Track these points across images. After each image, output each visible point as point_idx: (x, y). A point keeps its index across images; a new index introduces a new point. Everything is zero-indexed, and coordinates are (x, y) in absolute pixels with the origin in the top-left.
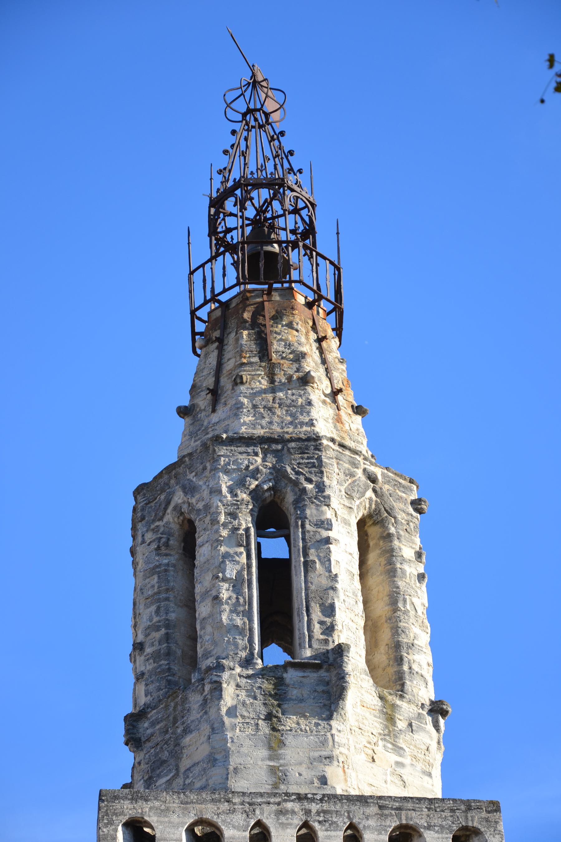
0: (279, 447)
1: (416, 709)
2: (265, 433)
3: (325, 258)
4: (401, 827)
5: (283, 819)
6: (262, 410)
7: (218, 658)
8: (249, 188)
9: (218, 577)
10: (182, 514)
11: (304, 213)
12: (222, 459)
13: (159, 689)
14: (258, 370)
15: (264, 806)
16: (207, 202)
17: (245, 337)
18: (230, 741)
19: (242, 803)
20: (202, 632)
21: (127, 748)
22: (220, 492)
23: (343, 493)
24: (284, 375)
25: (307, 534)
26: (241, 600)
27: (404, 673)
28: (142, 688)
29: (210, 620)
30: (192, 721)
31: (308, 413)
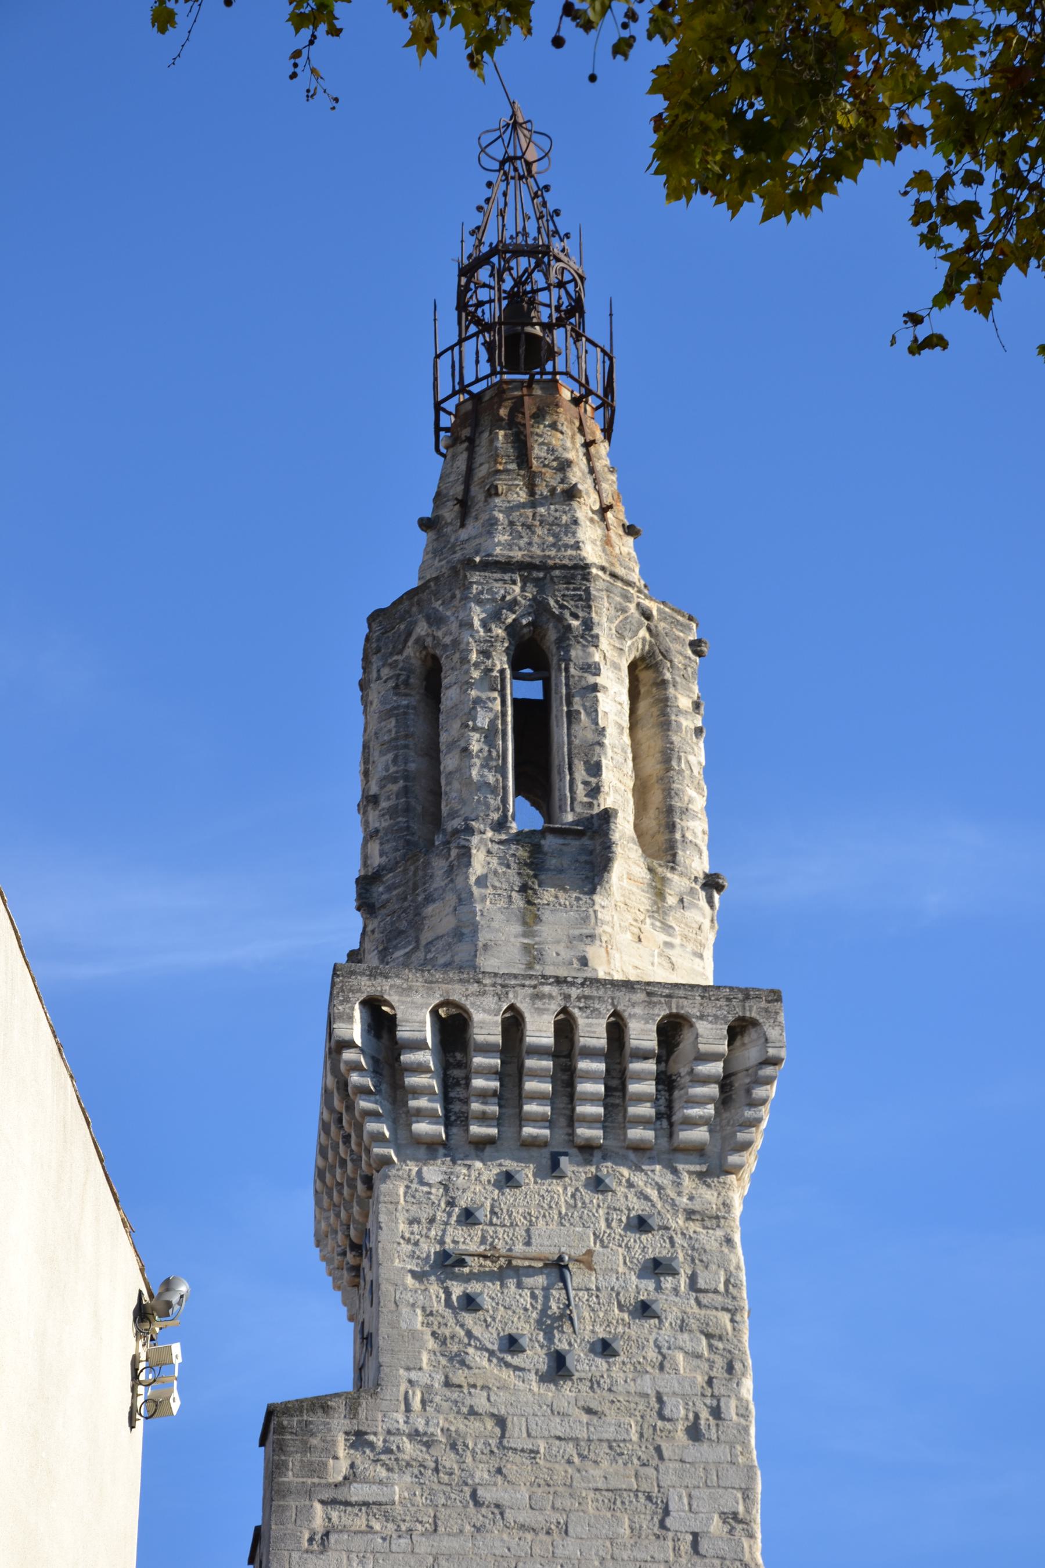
0: (541, 575)
1: (688, 882)
2: (523, 556)
3: (596, 345)
4: (670, 1016)
5: (539, 1004)
6: (520, 528)
7: (466, 819)
8: (508, 255)
9: (467, 726)
10: (425, 648)
11: (570, 287)
12: (475, 586)
13: (396, 850)
14: (515, 479)
15: (518, 989)
16: (456, 272)
17: (500, 438)
18: (479, 914)
19: (494, 985)
20: (448, 788)
21: (358, 914)
22: (471, 625)
23: (614, 631)
24: (547, 486)
25: (571, 679)
26: (494, 754)
27: (676, 841)
28: (374, 847)
29: (458, 775)
30: (435, 890)
31: (574, 533)
